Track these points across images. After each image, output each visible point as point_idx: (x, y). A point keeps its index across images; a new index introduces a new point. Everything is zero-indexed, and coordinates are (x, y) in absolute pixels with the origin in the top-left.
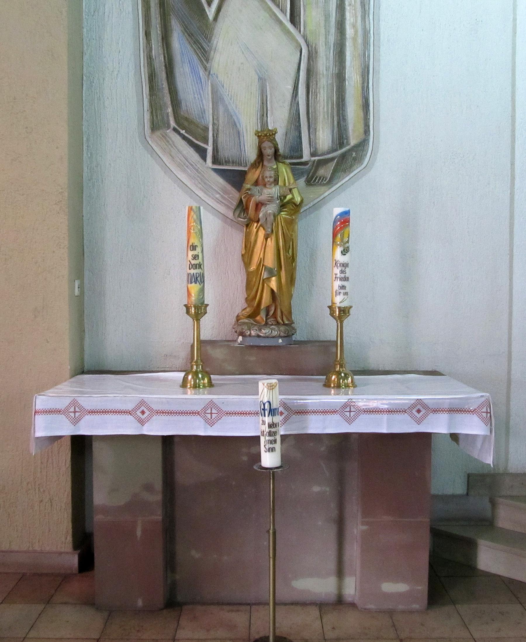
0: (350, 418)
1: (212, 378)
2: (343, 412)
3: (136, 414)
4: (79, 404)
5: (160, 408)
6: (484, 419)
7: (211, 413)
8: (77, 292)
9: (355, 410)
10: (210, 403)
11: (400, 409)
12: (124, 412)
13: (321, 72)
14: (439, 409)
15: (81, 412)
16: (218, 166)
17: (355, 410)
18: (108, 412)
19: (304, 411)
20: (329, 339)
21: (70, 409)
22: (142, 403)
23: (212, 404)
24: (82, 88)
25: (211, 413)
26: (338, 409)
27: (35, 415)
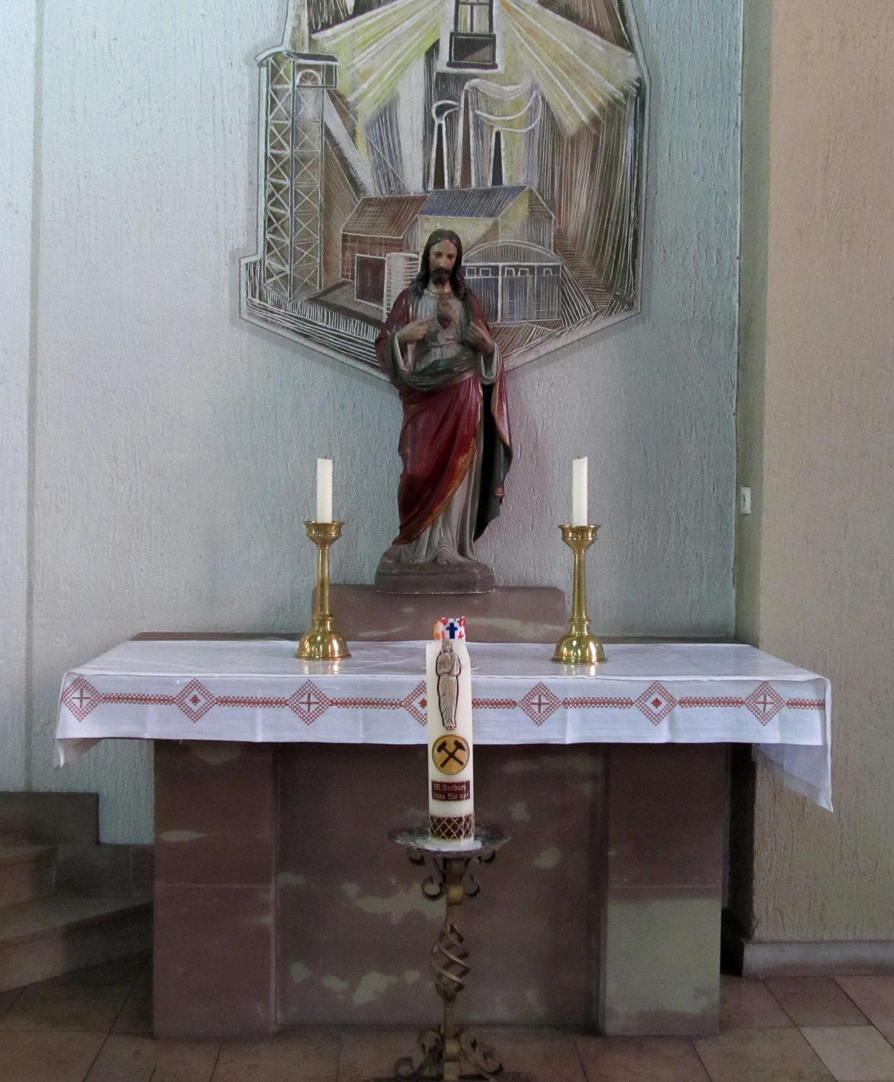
0: (320, 703)
1: (604, 648)
2: (297, 703)
3: (184, 703)
4: (186, 707)
5: (571, 695)
6: (321, 708)
7: (765, 703)
8: (747, 492)
9: (83, 708)
10: (211, 705)
11: (396, 700)
12: (244, 702)
13: (569, 125)
14: (392, 700)
15: (320, 703)
16: (480, 463)
17: (83, 708)
18: (382, 704)
19: (495, 702)
20: (545, 583)
21: (77, 706)
22: (656, 686)
23: (540, 690)
24: (741, 147)
25: (540, 704)
26: (403, 700)
27: (61, 702)
